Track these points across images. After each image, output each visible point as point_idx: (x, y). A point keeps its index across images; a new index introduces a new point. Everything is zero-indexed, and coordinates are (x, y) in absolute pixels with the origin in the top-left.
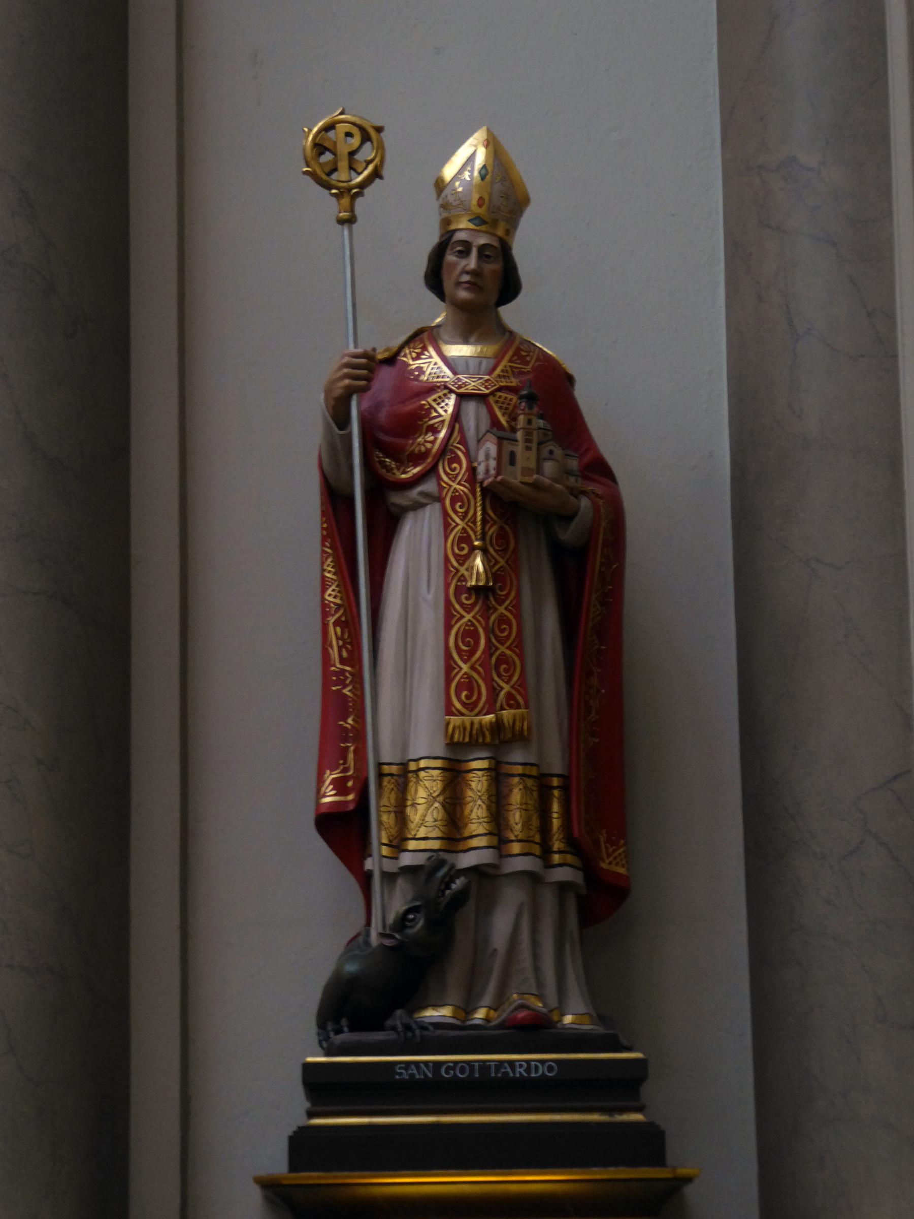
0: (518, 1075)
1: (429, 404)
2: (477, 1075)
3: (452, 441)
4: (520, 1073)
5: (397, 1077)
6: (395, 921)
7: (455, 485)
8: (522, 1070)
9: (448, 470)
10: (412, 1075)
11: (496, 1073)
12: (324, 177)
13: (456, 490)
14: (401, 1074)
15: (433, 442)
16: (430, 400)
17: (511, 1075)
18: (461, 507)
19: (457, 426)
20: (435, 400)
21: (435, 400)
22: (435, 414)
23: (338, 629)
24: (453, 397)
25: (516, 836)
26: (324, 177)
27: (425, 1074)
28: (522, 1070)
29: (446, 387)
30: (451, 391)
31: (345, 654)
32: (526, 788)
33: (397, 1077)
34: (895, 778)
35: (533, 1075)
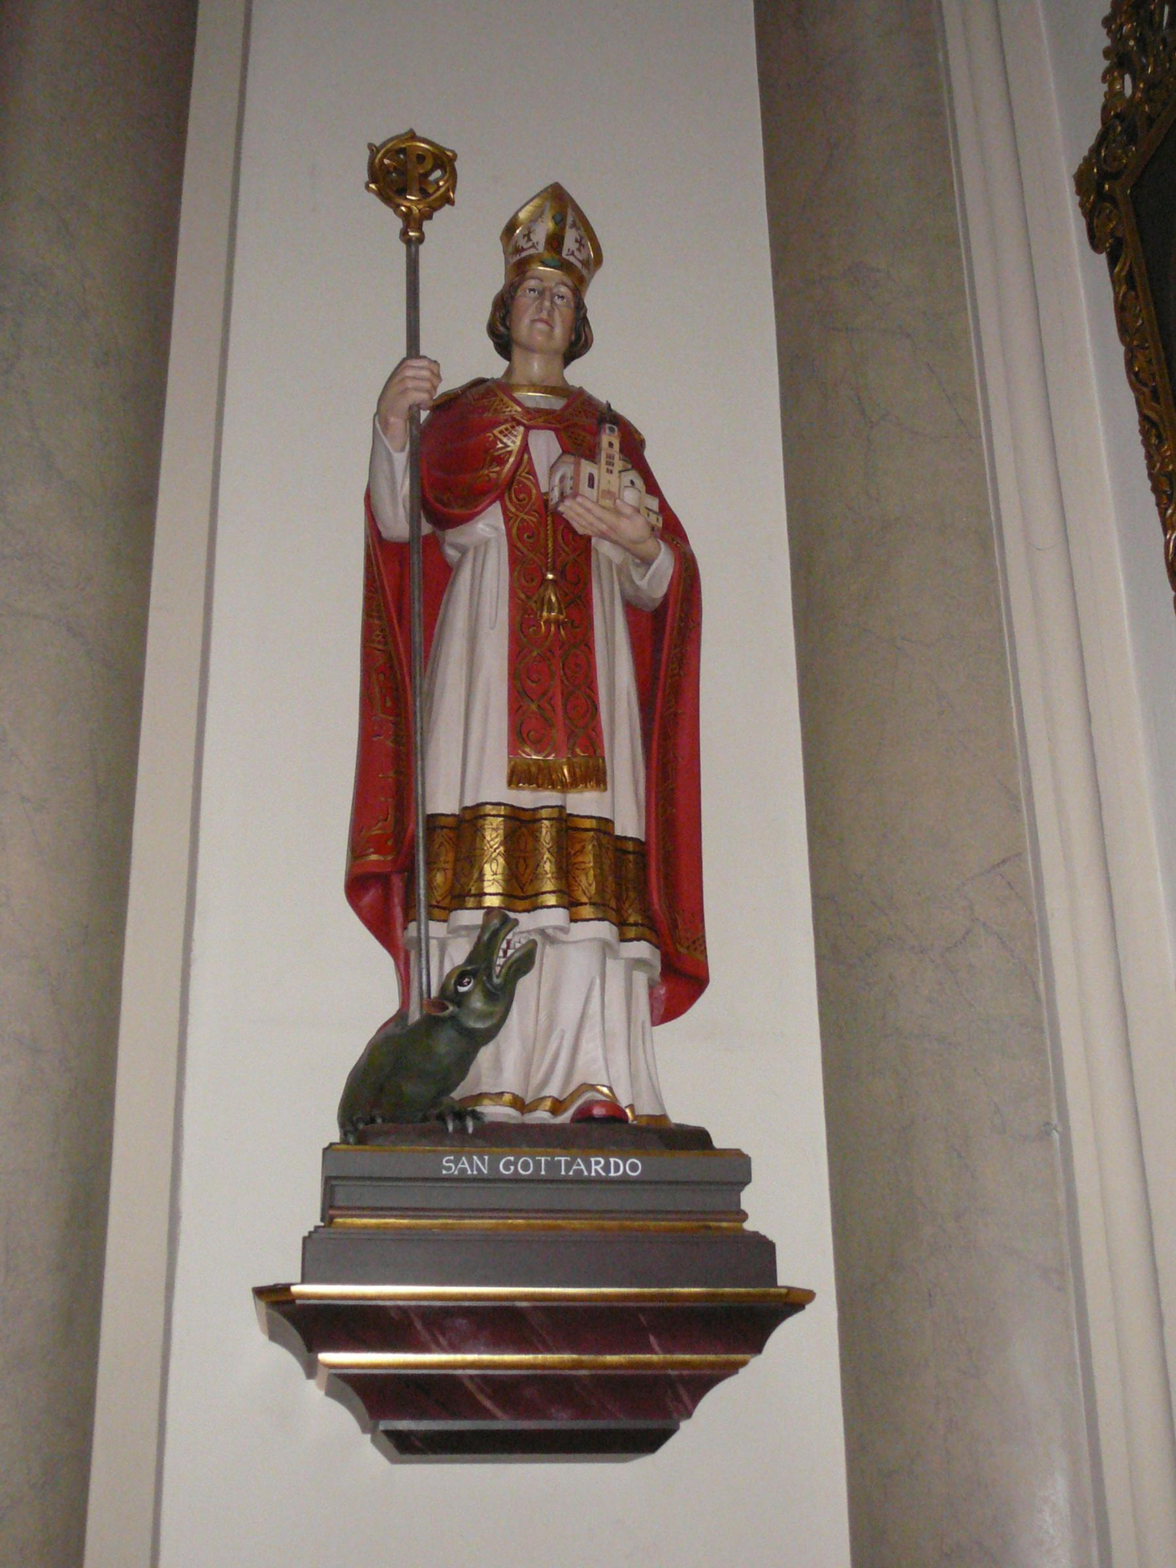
0: (593, 1174)
1: (495, 436)
2: (543, 1173)
3: (521, 470)
4: (596, 1171)
5: (444, 1172)
6: (444, 394)
7: (522, 515)
8: (598, 1168)
9: (514, 499)
10: (464, 1170)
11: (567, 1170)
12: (397, 882)
13: (523, 520)
14: (449, 1168)
15: (498, 473)
16: (496, 432)
17: (586, 1173)
18: (529, 537)
19: (526, 456)
20: (501, 432)
21: (501, 432)
22: (500, 445)
23: (382, 677)
24: (521, 429)
25: (590, 899)
26: (397, 882)
27: (479, 1169)
28: (598, 1168)
29: (514, 419)
30: (519, 423)
31: (389, 704)
32: (600, 845)
33: (444, 1172)
34: (1004, 862)
35: (612, 1174)
